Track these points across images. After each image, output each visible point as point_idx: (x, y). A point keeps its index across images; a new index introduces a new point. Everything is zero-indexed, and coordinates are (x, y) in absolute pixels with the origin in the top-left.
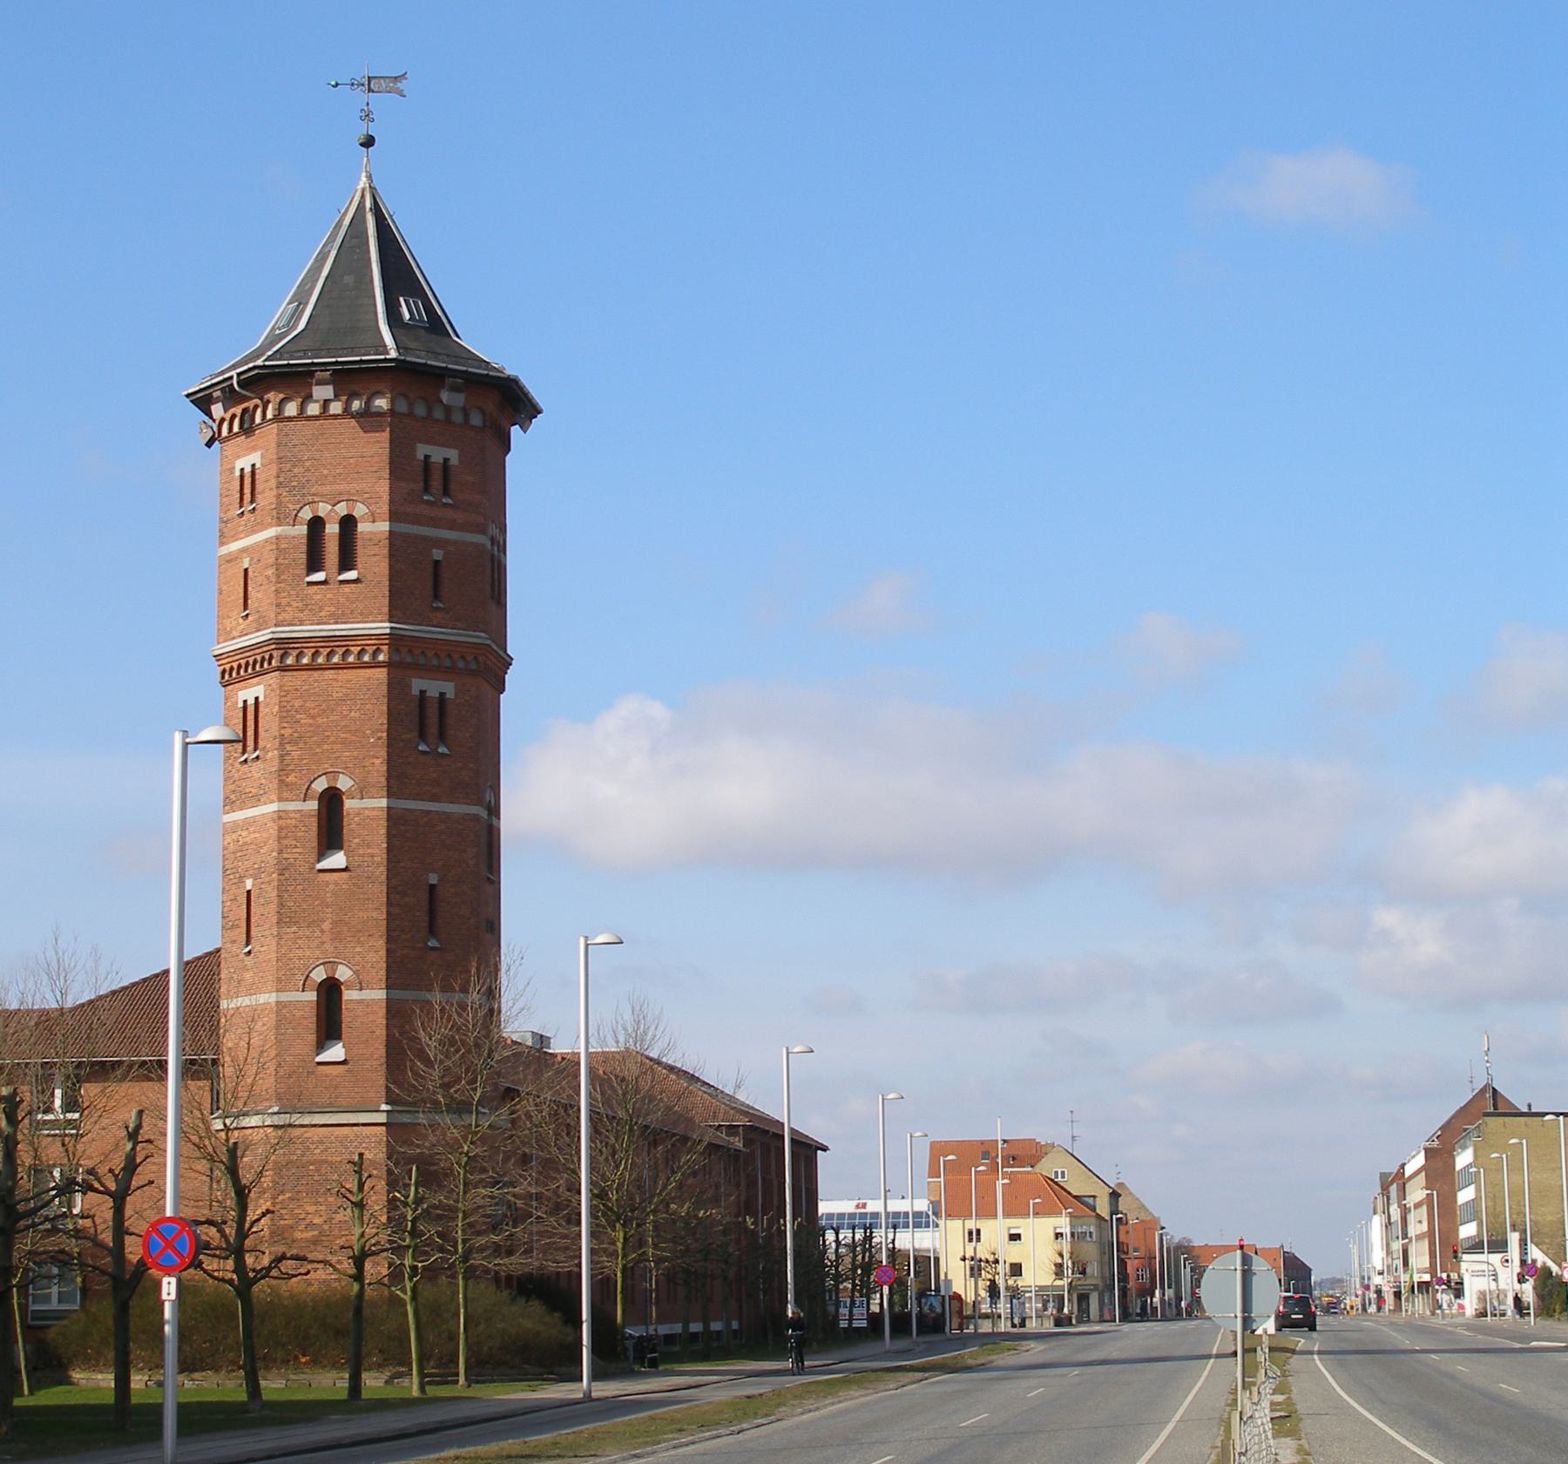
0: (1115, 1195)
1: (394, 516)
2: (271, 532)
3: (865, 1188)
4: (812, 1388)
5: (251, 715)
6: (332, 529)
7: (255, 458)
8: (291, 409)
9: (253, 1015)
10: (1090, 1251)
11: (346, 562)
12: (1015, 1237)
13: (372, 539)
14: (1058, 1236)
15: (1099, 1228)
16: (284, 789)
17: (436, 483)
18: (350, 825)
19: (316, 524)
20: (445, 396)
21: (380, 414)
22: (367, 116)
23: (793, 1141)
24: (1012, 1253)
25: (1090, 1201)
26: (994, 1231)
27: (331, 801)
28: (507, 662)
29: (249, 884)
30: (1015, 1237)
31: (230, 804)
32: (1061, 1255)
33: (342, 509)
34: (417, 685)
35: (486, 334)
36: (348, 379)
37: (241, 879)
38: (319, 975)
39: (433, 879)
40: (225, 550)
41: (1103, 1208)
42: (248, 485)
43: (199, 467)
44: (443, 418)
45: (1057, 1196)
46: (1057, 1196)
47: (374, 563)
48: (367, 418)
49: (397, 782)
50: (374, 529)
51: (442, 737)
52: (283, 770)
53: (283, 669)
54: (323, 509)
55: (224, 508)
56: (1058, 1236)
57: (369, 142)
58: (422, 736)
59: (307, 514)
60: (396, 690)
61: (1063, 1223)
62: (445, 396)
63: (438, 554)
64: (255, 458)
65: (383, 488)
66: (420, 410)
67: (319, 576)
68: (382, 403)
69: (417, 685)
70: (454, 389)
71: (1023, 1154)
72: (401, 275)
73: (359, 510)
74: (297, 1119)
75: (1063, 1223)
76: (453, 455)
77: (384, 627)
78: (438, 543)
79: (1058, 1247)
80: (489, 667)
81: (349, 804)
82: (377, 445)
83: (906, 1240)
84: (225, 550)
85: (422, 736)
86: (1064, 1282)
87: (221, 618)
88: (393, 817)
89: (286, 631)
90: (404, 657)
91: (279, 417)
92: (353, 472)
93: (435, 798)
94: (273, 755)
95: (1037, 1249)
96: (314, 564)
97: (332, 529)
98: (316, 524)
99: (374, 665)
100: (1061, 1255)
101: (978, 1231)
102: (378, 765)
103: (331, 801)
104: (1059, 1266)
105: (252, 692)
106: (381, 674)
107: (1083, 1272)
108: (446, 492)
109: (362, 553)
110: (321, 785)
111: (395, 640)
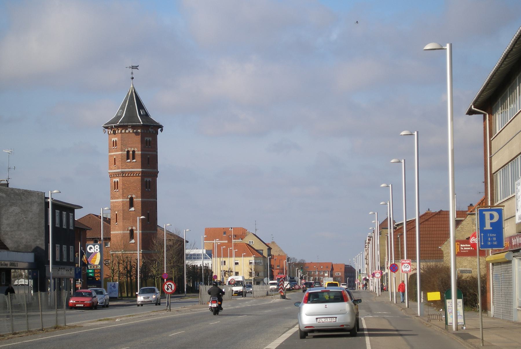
0: (270, 249)
1: (142, 151)
2: (120, 153)
3: (198, 254)
4: (266, 270)
5: (116, 184)
6: (131, 153)
7: (116, 139)
8: (123, 131)
9: (116, 235)
10: (261, 268)
11: (133, 158)
12: (237, 264)
13: (138, 154)
14: (250, 263)
15: (264, 261)
16: (123, 197)
17: (148, 144)
18: (135, 203)
19: (128, 152)
20: (150, 130)
21: (139, 133)
22: (132, 73)
23: (166, 233)
24: (235, 269)
25: (261, 251)
26: (230, 262)
27: (131, 199)
28: (158, 172)
29: (116, 212)
30: (237, 264)
31: (112, 198)
32: (251, 269)
33: (133, 149)
34: (146, 179)
35: (155, 117)
36: (133, 127)
37: (115, 212)
38: (130, 228)
39: (148, 212)
40: (110, 154)
41: (265, 254)
42: (115, 144)
43: (104, 139)
44: (149, 131)
45: (250, 250)
46: (250, 250)
47: (138, 159)
48: (137, 133)
49: (143, 197)
50: (138, 153)
51: (149, 188)
52: (123, 194)
53: (123, 176)
54: (129, 149)
55: (110, 147)
56: (250, 263)
57: (133, 78)
58: (146, 188)
59: (126, 150)
60: (142, 180)
61: (252, 259)
62: (150, 130)
63: (149, 156)
64: (116, 139)
65: (140, 146)
66: (145, 131)
67: (129, 161)
68: (139, 131)
69: (146, 179)
70: (152, 128)
71: (241, 234)
72: (141, 106)
73: (136, 149)
74: (127, 252)
75: (252, 259)
76: (151, 139)
77: (140, 170)
78: (149, 154)
79: (250, 267)
80: (155, 174)
81: (134, 200)
82: (138, 138)
83: (198, 263)
84: (110, 154)
85: (146, 188)
86: (252, 278)
87: (110, 166)
88: (142, 202)
89: (123, 170)
90: (144, 175)
91: (121, 133)
92: (135, 145)
93: (148, 198)
94: (121, 191)
95: (243, 267)
96: (128, 159)
97: (131, 153)
98: (128, 152)
99: (139, 176)
100: (251, 269)
101: (225, 262)
102: (139, 193)
103: (131, 199)
104: (251, 273)
105: (116, 180)
106: (140, 178)
107: (258, 275)
108: (150, 145)
109: (136, 157)
110: (130, 196)
111: (142, 172)
